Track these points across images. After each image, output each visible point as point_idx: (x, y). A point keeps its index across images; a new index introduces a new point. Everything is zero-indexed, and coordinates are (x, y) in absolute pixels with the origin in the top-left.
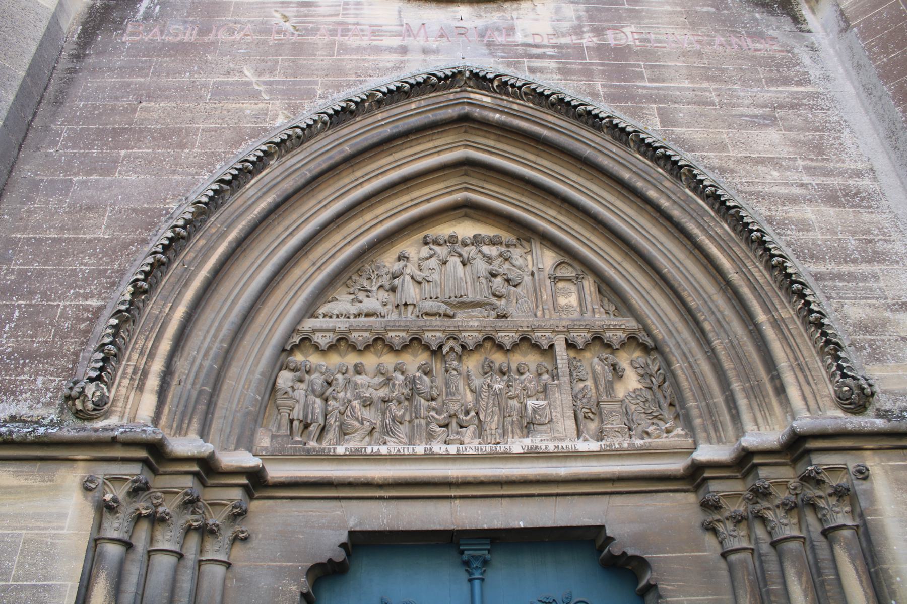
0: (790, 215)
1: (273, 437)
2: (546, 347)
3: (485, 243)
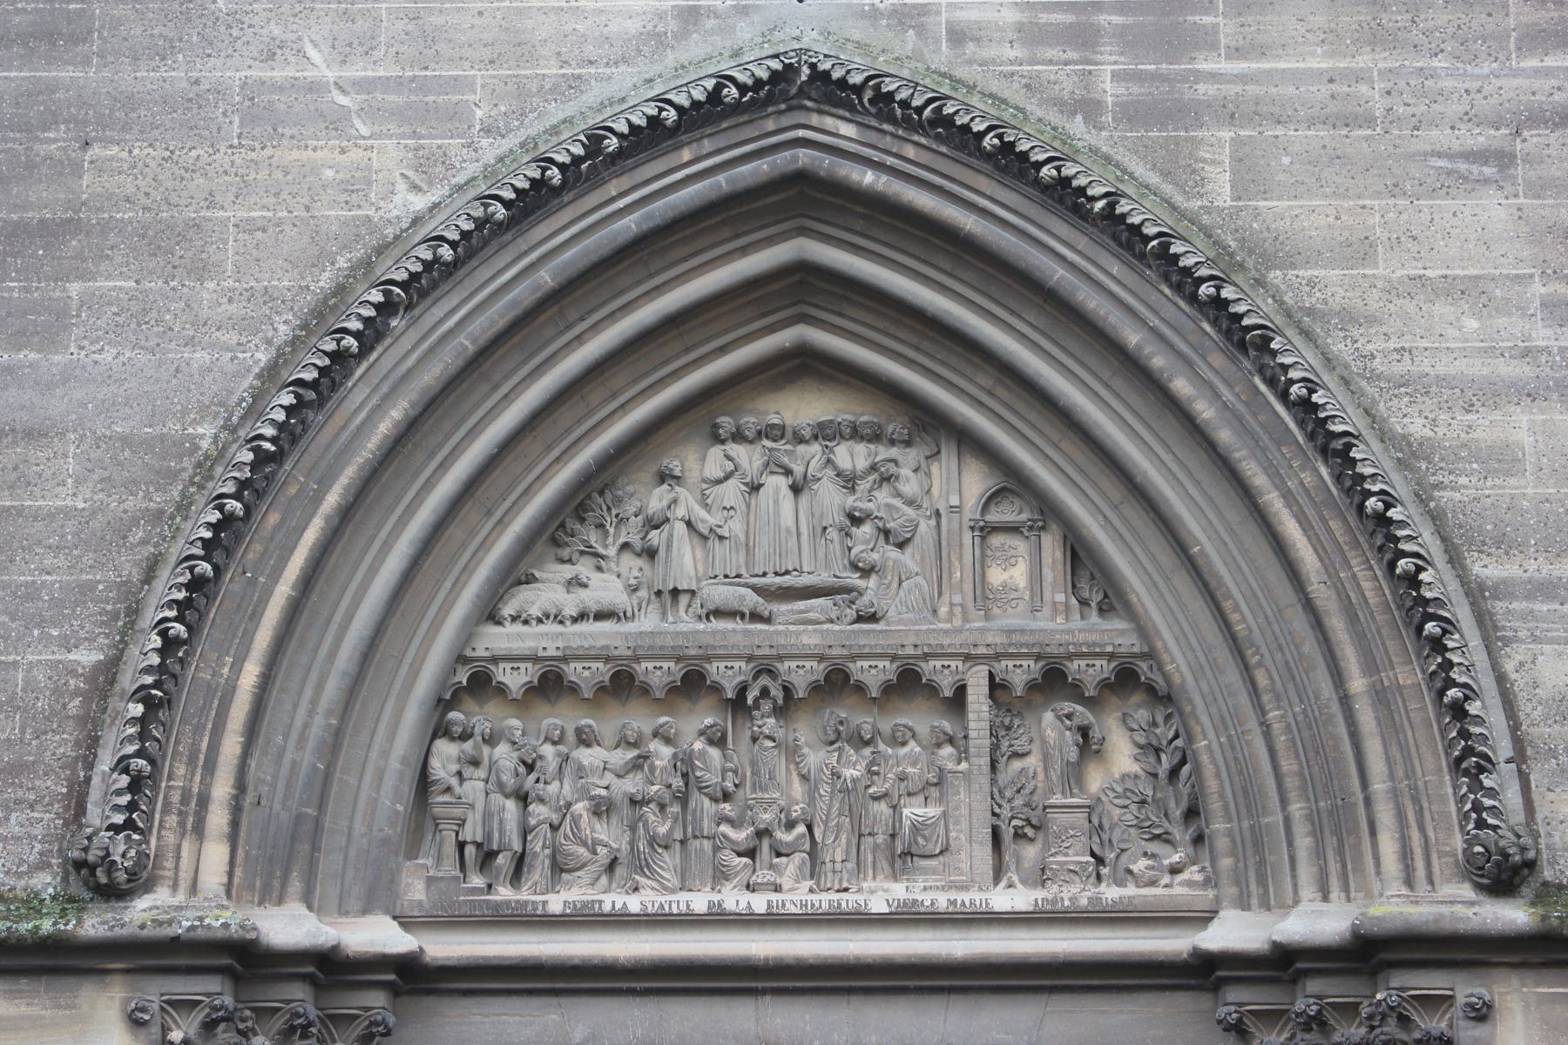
0: (1478, 434)
1: (430, 881)
2: (948, 693)
3: (842, 436)
